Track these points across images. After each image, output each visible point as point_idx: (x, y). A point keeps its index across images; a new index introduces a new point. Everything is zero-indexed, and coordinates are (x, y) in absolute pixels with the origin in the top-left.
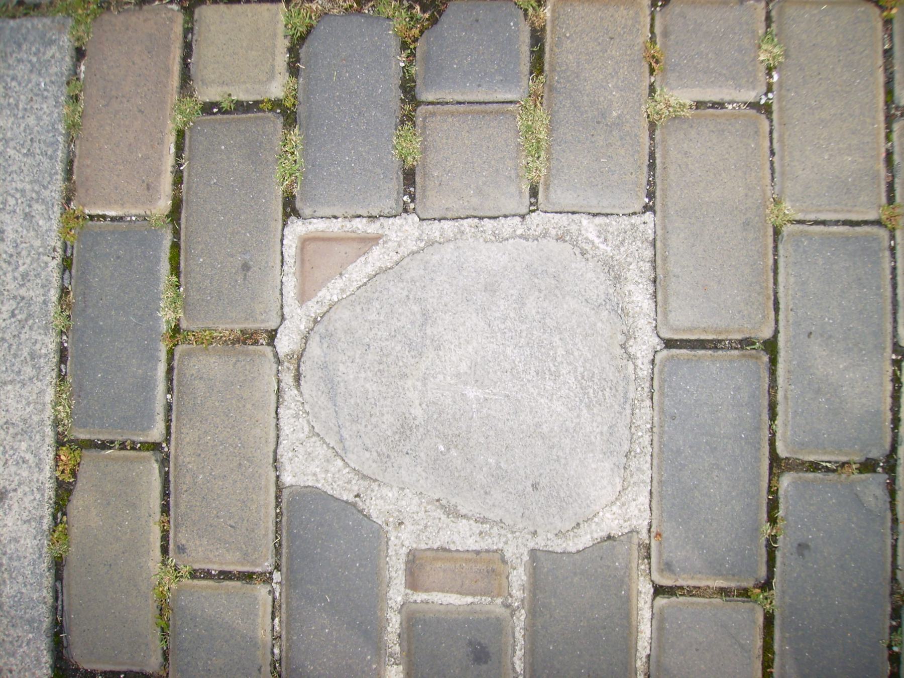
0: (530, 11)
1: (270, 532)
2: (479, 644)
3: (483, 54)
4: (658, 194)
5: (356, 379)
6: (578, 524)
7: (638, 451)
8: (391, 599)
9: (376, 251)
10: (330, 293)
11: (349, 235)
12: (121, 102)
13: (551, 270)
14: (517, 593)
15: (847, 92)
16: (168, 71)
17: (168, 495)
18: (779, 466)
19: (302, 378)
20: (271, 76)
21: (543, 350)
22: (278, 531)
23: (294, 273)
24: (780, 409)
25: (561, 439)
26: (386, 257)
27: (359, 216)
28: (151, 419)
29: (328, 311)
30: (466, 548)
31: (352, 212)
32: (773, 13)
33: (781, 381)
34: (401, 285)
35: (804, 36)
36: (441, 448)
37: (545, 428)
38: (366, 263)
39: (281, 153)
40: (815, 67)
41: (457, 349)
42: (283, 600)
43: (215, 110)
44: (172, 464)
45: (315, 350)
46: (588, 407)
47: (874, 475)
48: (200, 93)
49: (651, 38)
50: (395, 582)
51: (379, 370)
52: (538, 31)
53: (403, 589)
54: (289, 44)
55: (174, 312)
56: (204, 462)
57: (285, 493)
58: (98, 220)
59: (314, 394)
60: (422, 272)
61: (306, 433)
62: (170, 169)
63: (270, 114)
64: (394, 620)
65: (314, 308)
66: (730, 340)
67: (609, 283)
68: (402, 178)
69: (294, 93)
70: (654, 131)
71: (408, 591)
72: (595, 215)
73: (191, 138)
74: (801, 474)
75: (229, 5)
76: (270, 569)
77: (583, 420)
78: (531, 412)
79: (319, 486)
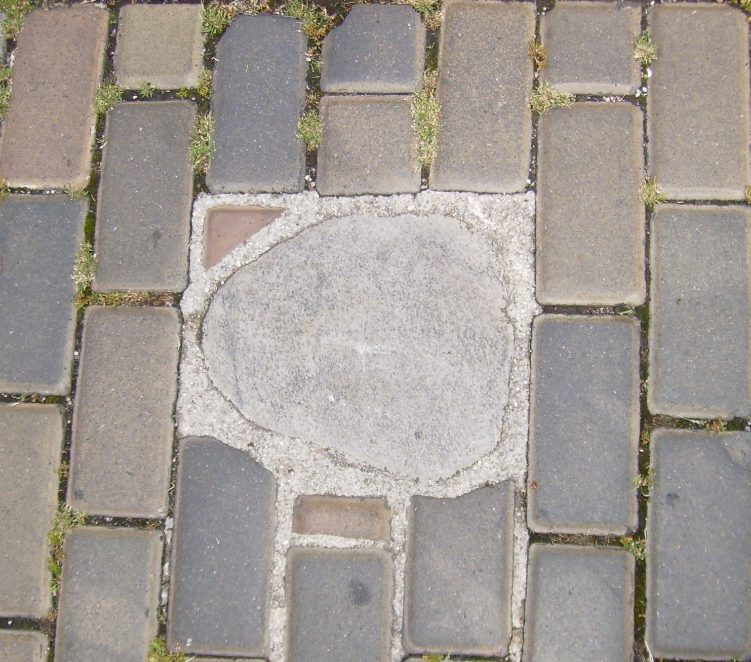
0: (427, 14)
1: (165, 479)
2: (361, 585)
3: (382, 50)
4: (539, 175)
5: (254, 335)
6: (458, 472)
7: (516, 404)
8: (278, 543)
9: (278, 223)
10: (235, 258)
11: (255, 208)
12: (48, 88)
13: (439, 241)
14: (398, 537)
15: (715, 86)
16: (93, 61)
17: (69, 446)
18: (650, 423)
19: (204, 337)
20: (188, 67)
21: (429, 311)
22: (173, 479)
23: (202, 242)
24: (651, 370)
25: (443, 391)
26: (287, 228)
27: (265, 192)
28: (58, 374)
29: (231, 276)
30: (352, 494)
31: (257, 188)
32: (648, 18)
33: (651, 344)
34: (299, 252)
35: (675, 37)
36: (332, 398)
37: (429, 381)
38: (269, 233)
39: (195, 135)
40: (685, 64)
41: (350, 309)
42: (174, 545)
43: (135, 97)
44: (75, 416)
45: (218, 309)
46: (469, 362)
47: (742, 432)
48: (121, 82)
49: (536, 39)
50: (283, 526)
51: (277, 327)
52: (433, 32)
53: (290, 533)
54: (205, 40)
55: (86, 275)
56: (107, 411)
57: (182, 443)
58: (19, 192)
59: (215, 350)
60: (320, 241)
61: (205, 387)
62: (90, 148)
63: (186, 102)
64: (280, 563)
65: (218, 273)
66: (605, 307)
67: (491, 253)
68: (304, 159)
69: (209, 83)
70: (537, 120)
71: (296, 535)
72: (480, 194)
73: (111, 121)
74: (671, 430)
75: (152, 5)
76: (163, 515)
77: (464, 375)
78: (416, 367)
79: (215, 435)
